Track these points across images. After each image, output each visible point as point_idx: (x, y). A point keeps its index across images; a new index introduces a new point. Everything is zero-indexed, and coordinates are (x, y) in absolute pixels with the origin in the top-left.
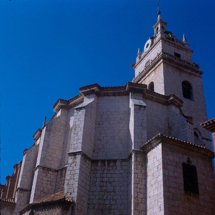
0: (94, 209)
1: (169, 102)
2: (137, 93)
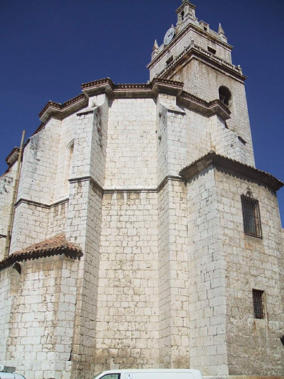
0: (109, 261)
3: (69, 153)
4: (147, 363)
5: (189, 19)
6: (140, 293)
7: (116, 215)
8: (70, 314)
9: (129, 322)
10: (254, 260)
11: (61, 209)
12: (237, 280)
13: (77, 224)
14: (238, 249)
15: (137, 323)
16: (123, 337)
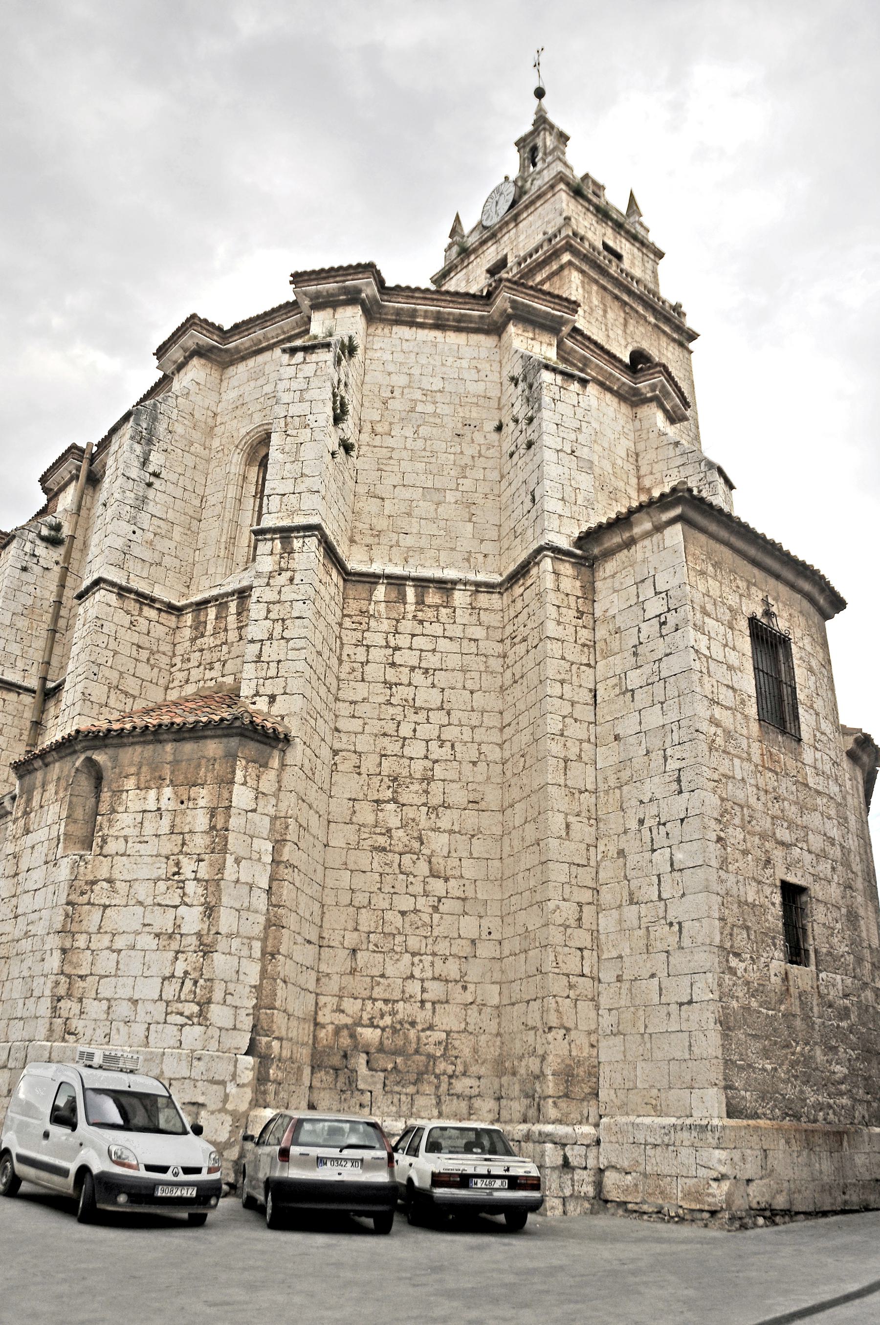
0: (359, 774)
1: (644, 391)
2: (537, 331)
3: (243, 467)
4: (464, 1074)
5: (558, 162)
6: (449, 873)
7: (381, 647)
8: (252, 917)
9: (414, 954)
10: (783, 800)
11: (216, 619)
12: (745, 852)
13: (275, 657)
14: (746, 764)
15: (437, 959)
16: (397, 995)
